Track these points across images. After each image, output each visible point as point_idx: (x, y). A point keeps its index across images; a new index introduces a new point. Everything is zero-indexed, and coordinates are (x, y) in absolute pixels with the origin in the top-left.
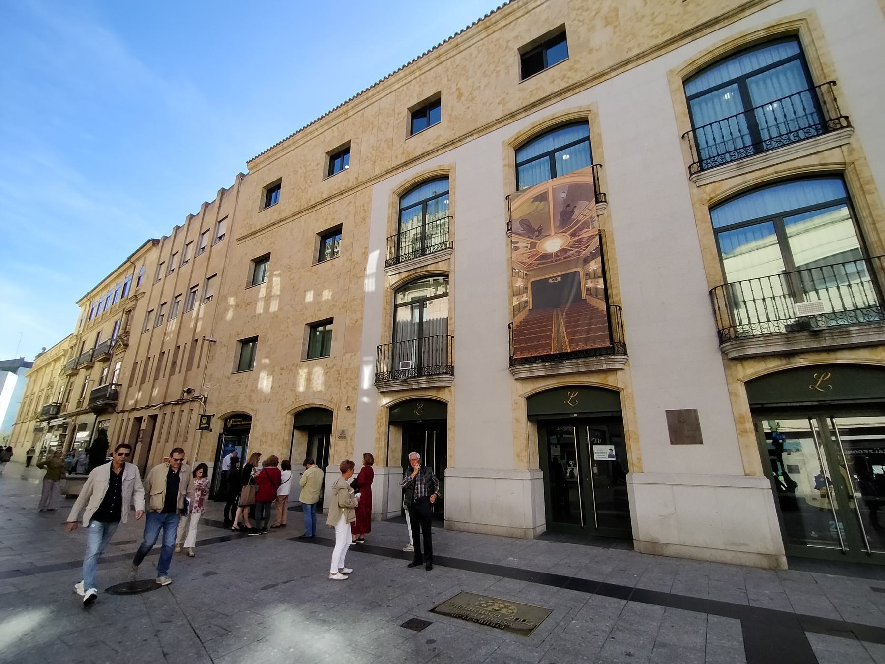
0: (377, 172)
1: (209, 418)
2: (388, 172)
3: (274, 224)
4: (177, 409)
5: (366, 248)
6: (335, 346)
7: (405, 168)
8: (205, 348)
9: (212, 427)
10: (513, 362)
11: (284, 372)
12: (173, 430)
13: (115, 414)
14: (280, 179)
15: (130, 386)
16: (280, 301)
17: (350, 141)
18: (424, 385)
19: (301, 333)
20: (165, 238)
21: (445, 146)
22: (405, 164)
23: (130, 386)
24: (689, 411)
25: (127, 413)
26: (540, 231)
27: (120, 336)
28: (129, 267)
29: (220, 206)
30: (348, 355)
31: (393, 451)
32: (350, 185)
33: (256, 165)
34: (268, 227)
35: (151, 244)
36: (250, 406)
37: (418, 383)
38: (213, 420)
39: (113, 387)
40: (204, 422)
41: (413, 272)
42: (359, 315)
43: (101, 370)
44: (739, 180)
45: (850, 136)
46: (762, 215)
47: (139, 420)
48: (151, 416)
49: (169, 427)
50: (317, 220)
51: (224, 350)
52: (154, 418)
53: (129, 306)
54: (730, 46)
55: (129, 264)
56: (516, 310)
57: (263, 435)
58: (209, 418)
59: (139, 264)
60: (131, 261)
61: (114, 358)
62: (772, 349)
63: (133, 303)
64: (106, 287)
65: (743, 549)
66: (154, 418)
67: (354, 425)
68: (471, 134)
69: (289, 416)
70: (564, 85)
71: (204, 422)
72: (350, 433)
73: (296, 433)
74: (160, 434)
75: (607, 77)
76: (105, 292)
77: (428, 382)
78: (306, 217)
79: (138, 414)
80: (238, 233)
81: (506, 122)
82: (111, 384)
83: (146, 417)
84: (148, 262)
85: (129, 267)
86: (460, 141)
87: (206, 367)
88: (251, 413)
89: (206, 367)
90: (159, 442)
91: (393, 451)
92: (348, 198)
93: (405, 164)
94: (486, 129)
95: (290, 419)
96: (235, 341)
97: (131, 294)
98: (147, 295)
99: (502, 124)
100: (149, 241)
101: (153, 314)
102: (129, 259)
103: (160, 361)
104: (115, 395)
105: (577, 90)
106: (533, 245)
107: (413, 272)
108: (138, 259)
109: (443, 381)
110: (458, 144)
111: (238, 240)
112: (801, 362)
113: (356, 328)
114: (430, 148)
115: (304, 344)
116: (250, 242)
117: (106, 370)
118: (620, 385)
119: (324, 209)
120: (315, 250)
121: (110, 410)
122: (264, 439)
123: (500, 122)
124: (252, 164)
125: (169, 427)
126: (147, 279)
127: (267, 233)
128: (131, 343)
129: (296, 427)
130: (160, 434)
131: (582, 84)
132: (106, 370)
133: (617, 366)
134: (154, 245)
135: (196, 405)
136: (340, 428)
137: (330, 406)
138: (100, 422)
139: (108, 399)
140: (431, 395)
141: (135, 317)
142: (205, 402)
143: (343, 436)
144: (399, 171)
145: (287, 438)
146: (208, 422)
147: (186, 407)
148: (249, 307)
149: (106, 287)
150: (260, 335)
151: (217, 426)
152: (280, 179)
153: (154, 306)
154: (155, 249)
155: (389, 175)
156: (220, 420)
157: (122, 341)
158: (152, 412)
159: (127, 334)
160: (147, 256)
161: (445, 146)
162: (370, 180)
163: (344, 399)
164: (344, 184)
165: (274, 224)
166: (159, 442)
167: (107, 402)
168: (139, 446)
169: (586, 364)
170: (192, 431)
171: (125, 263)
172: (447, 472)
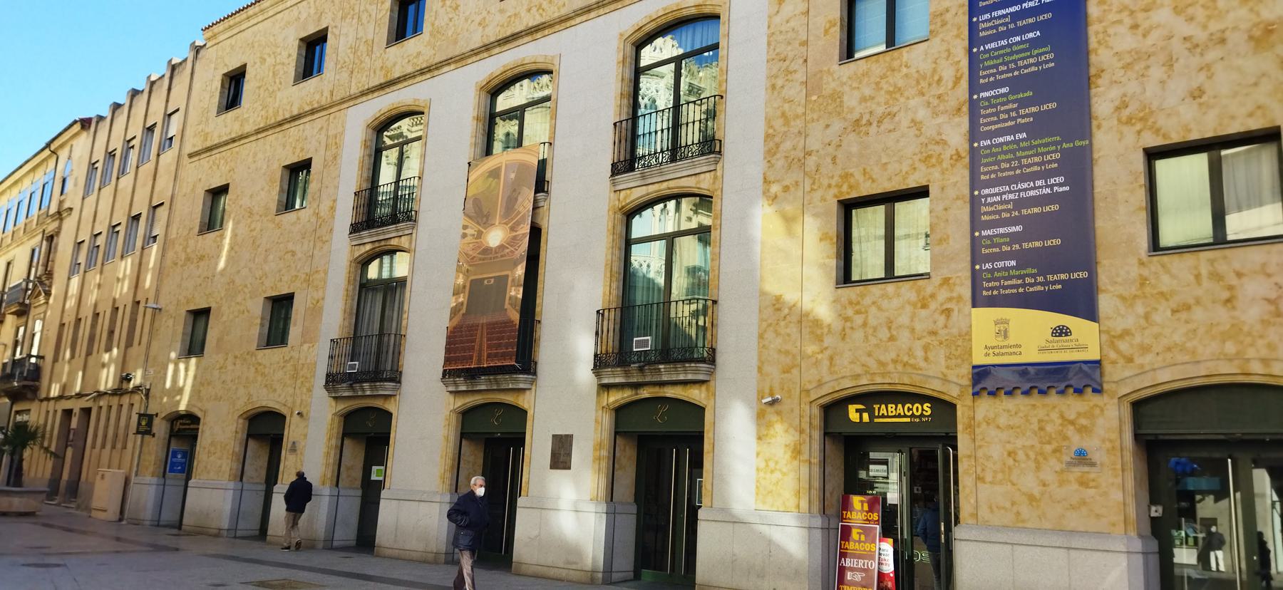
0: (354, 90)
1: (150, 418)
2: (363, 94)
3: (234, 141)
4: (115, 401)
5: (335, 201)
6: (294, 332)
7: (382, 92)
8: (148, 316)
9: (155, 430)
10: (445, 374)
11: (238, 362)
12: (121, 431)
13: (36, 403)
14: (245, 65)
15: (55, 360)
16: (233, 268)
17: (327, 29)
18: (368, 393)
19: (257, 309)
20: (101, 118)
21: (422, 72)
22: (381, 87)
23: (55, 360)
24: (567, 436)
25: (52, 402)
26: (487, 216)
27: (39, 278)
28: (49, 157)
29: (169, 89)
30: (306, 346)
31: (348, 469)
32: (323, 103)
33: (214, 36)
34: (226, 143)
35: (77, 127)
36: (199, 405)
37: (363, 390)
38: (156, 421)
39: (33, 360)
40: (144, 423)
41: (377, 245)
42: (320, 293)
43: (13, 330)
44: (643, 191)
45: (717, 163)
46: (656, 232)
47: (68, 413)
48: (82, 409)
49: (106, 427)
50: (284, 146)
51: (170, 322)
52: (87, 411)
53: (51, 227)
54: (670, 18)
55: (47, 152)
56: (454, 312)
57: (212, 444)
58: (150, 418)
59: (63, 154)
60: (51, 148)
61: (33, 312)
62: (618, 380)
63: (56, 224)
64: (16, 183)
65: (574, 567)
66: (87, 411)
67: (306, 436)
68: (447, 62)
69: (241, 421)
70: (538, 20)
71: (144, 423)
72: (299, 447)
73: (252, 443)
74: (95, 436)
75: (573, 22)
76: (15, 191)
77: (372, 388)
78: (273, 138)
79: (67, 405)
80: (191, 145)
81: (481, 56)
82: (30, 356)
83: (76, 410)
84: (76, 155)
85: (49, 157)
86: (437, 69)
87: (149, 344)
88: (199, 414)
89: (149, 344)
90: (93, 447)
91: (348, 469)
92: (319, 121)
93: (381, 87)
94: (459, 60)
95: (242, 425)
96: (183, 313)
97: (53, 209)
98: (75, 214)
99: (478, 57)
100: (75, 122)
101: (85, 247)
102: (48, 145)
103: (94, 326)
104: (36, 372)
105: (546, 32)
106: (480, 235)
107: (377, 245)
108: (61, 146)
109: (386, 389)
110: (436, 73)
111: (190, 156)
112: (645, 393)
113: (316, 311)
114: (410, 69)
115: (262, 325)
116: (205, 161)
117: (22, 330)
118: (526, 406)
119: (293, 131)
120: (281, 190)
121: (29, 395)
122: (212, 449)
123: (476, 54)
124: (209, 33)
125: (106, 427)
126: (76, 185)
127: (225, 153)
128: (53, 292)
129: (250, 435)
130: (95, 436)
131: (551, 26)
132: (22, 330)
133: (522, 386)
134: (83, 127)
135: (136, 398)
136: (291, 440)
137: (284, 411)
138: (18, 412)
139: (26, 379)
140: (378, 403)
141: (60, 248)
142: (147, 395)
143: (293, 449)
144: (376, 94)
145: (238, 449)
146: (150, 424)
147: (126, 400)
148: (202, 264)
149: (16, 183)
150: (213, 306)
151: (160, 427)
152: (245, 65)
153: (85, 236)
154: (84, 134)
155: (364, 98)
156: (164, 422)
157: (42, 282)
158: (84, 403)
159: (49, 274)
160: (74, 142)
161: (422, 72)
162: (343, 101)
163: (298, 402)
164: (317, 97)
165: (234, 141)
166: (93, 447)
167: (26, 383)
168: (69, 452)
169: (497, 382)
170: (131, 436)
171: (43, 150)
172: (521, 501)
